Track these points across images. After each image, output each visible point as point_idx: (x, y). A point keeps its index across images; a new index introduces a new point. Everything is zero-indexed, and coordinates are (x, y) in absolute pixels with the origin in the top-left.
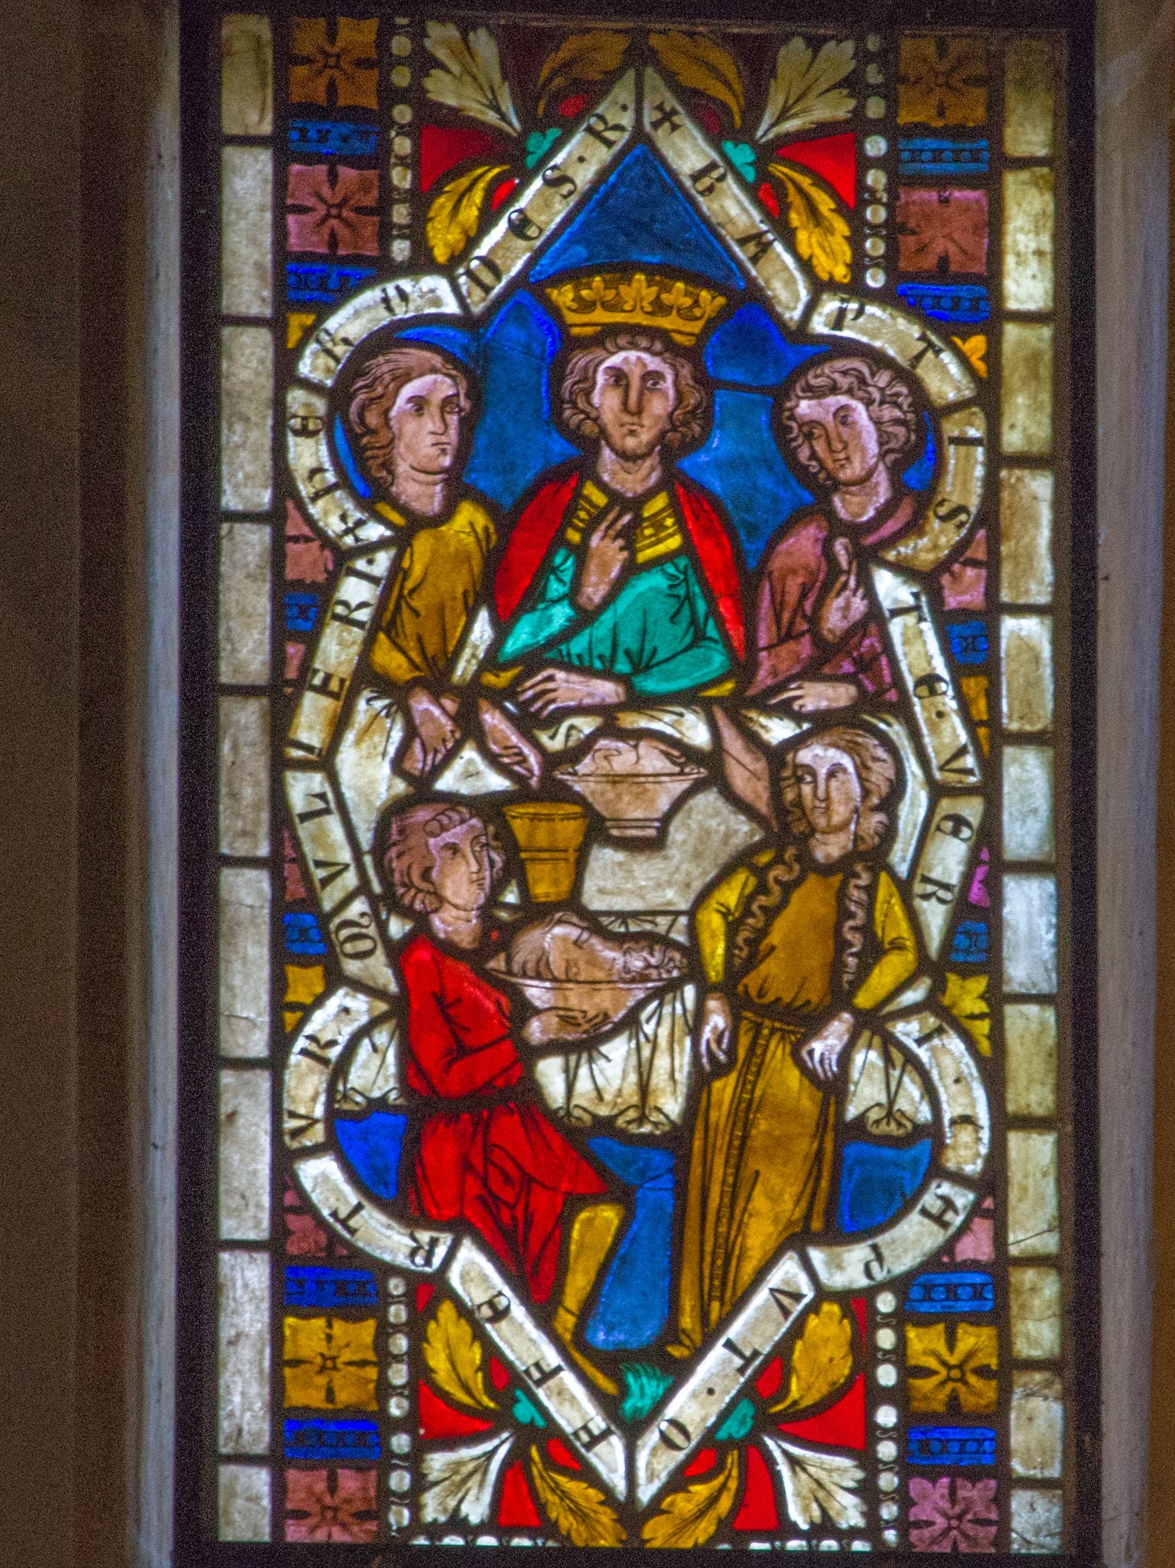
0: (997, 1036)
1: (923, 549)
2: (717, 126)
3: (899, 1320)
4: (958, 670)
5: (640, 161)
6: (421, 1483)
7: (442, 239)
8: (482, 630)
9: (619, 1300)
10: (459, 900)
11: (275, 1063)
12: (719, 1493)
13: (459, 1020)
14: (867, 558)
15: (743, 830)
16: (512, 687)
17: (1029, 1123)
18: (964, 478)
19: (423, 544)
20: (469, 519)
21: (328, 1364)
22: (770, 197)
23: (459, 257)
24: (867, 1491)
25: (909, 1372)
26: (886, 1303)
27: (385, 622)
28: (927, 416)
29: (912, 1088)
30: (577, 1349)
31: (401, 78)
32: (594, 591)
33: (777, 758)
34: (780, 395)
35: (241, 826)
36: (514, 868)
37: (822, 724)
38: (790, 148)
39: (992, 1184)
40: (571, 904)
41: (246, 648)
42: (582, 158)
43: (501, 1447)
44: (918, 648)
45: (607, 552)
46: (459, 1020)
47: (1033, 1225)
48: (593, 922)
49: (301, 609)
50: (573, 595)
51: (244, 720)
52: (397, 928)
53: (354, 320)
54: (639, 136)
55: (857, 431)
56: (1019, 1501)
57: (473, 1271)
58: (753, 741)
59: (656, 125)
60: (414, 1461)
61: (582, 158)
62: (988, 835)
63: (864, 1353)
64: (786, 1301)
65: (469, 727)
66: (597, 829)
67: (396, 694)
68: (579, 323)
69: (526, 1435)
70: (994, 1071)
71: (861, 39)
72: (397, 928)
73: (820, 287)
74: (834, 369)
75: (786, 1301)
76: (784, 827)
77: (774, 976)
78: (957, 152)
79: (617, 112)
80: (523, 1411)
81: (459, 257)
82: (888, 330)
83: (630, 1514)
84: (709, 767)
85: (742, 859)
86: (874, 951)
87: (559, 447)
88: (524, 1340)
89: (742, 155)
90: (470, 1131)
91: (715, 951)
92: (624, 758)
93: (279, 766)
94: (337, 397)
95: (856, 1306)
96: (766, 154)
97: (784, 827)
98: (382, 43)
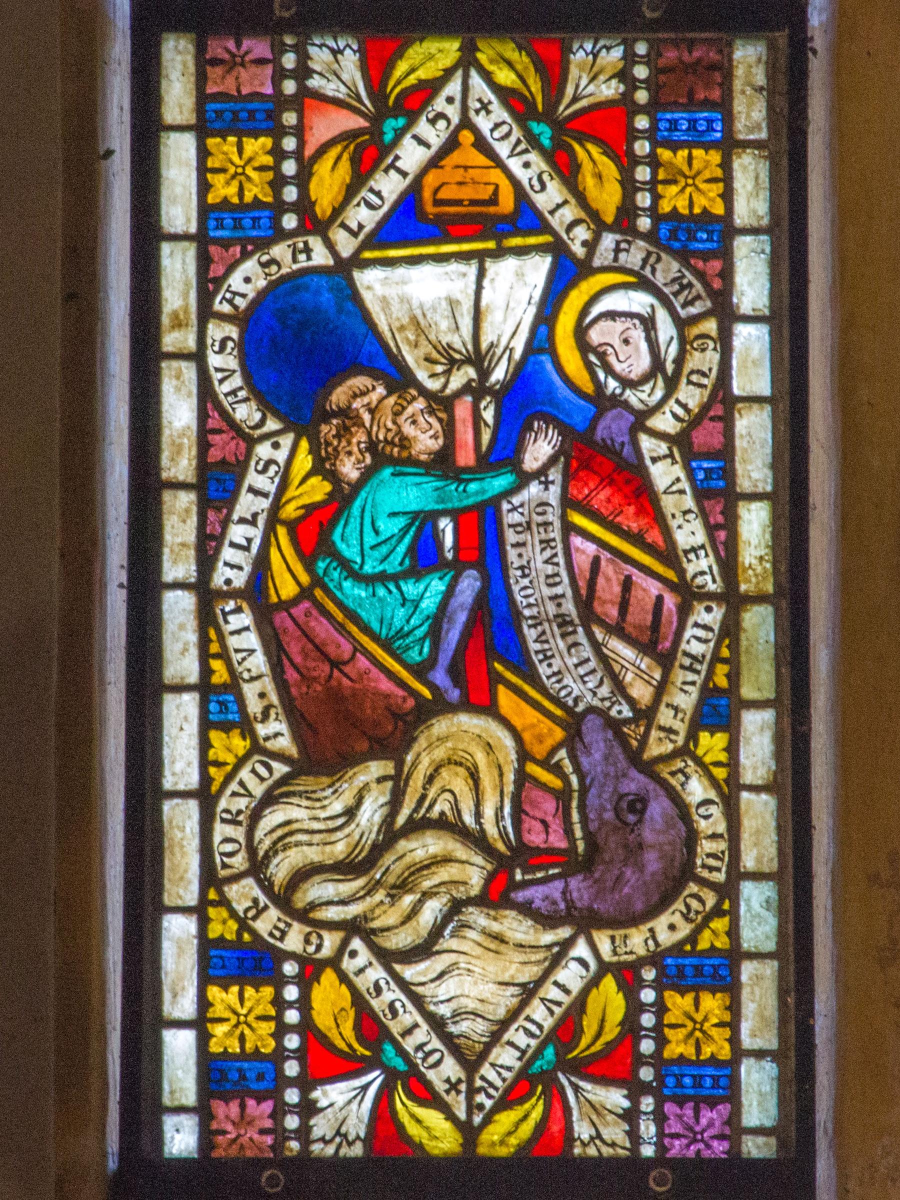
26: (649, 974)
59: (477, 112)
71: (629, 45)
95: (627, 975)
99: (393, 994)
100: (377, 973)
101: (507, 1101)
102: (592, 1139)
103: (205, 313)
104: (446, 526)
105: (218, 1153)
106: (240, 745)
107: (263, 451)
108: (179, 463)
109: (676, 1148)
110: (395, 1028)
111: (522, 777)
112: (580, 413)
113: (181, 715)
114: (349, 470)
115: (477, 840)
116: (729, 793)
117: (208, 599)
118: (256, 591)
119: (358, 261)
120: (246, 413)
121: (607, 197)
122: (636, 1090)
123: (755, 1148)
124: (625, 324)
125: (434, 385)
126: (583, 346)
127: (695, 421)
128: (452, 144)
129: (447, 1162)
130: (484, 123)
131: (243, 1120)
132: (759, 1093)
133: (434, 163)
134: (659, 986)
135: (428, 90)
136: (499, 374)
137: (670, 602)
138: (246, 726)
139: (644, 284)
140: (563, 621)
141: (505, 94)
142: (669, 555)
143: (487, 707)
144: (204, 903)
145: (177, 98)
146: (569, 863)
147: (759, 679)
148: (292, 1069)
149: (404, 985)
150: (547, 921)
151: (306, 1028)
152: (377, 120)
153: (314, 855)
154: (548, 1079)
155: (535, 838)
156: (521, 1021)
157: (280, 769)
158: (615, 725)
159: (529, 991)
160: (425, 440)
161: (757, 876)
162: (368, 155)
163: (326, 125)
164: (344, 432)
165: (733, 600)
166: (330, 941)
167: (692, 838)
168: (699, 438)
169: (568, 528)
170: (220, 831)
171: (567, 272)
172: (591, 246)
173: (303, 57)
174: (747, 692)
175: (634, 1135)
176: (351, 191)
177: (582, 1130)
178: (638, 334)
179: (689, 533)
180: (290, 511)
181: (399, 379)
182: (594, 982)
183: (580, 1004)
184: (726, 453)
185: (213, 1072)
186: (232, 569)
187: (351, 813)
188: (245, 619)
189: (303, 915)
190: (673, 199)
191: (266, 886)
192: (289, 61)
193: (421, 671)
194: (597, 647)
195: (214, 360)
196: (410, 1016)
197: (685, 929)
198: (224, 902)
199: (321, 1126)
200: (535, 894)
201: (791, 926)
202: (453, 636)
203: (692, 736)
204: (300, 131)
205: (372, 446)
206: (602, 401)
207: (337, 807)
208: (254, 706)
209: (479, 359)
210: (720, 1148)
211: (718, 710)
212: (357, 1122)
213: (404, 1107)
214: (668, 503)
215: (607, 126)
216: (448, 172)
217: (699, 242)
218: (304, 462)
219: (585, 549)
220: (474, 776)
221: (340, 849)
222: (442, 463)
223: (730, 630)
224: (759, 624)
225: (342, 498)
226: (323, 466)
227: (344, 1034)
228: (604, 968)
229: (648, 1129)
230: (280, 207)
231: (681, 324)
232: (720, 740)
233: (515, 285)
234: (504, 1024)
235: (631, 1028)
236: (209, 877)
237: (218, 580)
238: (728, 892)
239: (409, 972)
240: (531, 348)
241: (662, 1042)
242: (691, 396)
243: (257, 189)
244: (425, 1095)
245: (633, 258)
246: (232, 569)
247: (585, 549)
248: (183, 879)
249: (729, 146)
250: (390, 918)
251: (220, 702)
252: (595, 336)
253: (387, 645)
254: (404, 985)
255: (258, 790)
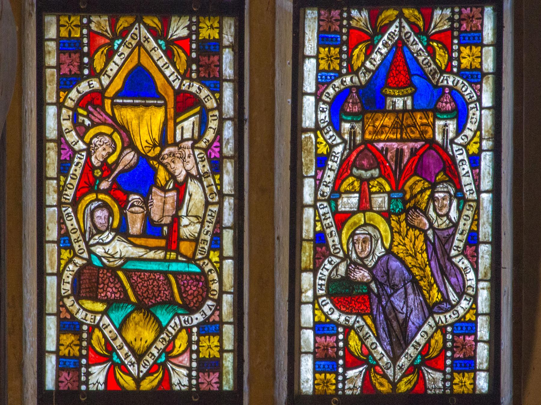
12: (413, 378)
24: (189, 376)
31: (345, 22)
59: (144, 41)
64: (360, 328)
75: (360, 328)
78: (474, 39)
98: (341, 14)
102: (178, 384)
105: (61, 389)
113: (51, 249)
129: (133, 391)
148: (84, 361)
154: (164, 364)
156: (163, 69)
165: (222, 120)
201: (237, 235)
213: (119, 374)
228: (182, 328)
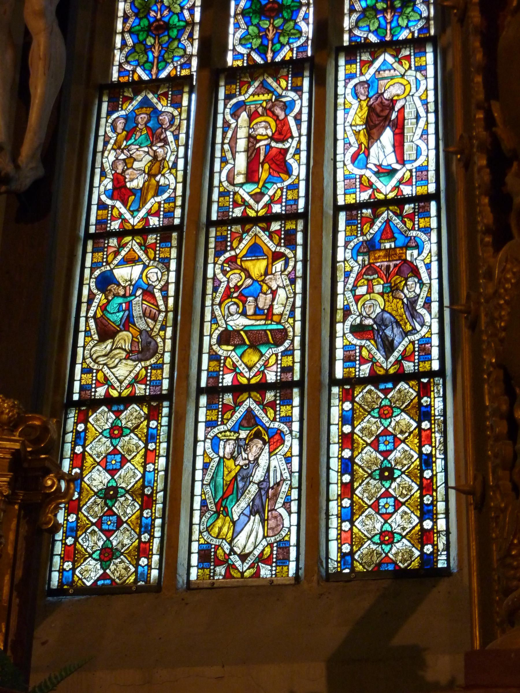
0: (176, 175)
1: (172, 129)
2: (154, 93)
3: (164, 204)
4: (175, 140)
5: (146, 98)
6: (111, 225)
7: (124, 108)
8: (125, 143)
9: (133, 205)
10: (120, 168)
11: (99, 187)
12: (143, 223)
13: (119, 182)
14: (166, 130)
15: (151, 158)
16: (127, 148)
17: (179, 183)
18: (177, 122)
19: (119, 136)
20: (125, 133)
21: (102, 215)
22: (159, 99)
23: (126, 109)
25: (164, 208)
26: (150, 368)
27: (115, 143)
28: (173, 117)
29: (167, 180)
30: (129, 210)
32: (137, 138)
33: (155, 152)
34: (158, 117)
35: (98, 165)
36: (126, 165)
37: (160, 147)
38: (161, 94)
39: (175, 189)
40: (132, 168)
41: (100, 147)
42: (139, 98)
43: (120, 221)
44: (170, 138)
45: (138, 134)
46: (119, 182)
47: (179, 192)
48: (134, 169)
49: (106, 143)
50: (135, 138)
51: (99, 155)
52: (113, 172)
53: (114, 116)
54: (146, 95)
55: (166, 119)
56: (175, 220)
57: (118, 204)
58: (152, 149)
60: (110, 223)
61: (139, 98)
62: (177, 156)
63: (160, 207)
65: (122, 152)
66: (135, 160)
67: (115, 150)
68: (138, 113)
69: (123, 219)
70: (176, 178)
72: (113, 172)
73: (163, 106)
74: (164, 114)
76: (155, 157)
77: (153, 172)
79: (143, 94)
80: (123, 217)
81: (126, 109)
82: (170, 109)
83: (133, 226)
84: (148, 153)
85: (151, 161)
86: (164, 168)
87: (135, 125)
88: (123, 210)
89: (156, 96)
90: (120, 191)
91: (147, 171)
92: (138, 153)
93: (102, 158)
94: (112, 124)
95: (146, 368)
96: (158, 95)
97: (155, 157)
99: (110, 374)
100: (108, 371)
101: (126, 388)
103: (91, 278)
104: (124, 305)
106: (90, 339)
107: (97, 296)
108: (85, 299)
109: (152, 393)
110: (110, 379)
111: (132, 340)
112: (145, 287)
113: (81, 335)
114: (110, 298)
115: (125, 350)
116: (164, 340)
117: (87, 318)
118: (94, 317)
119: (114, 268)
120: (95, 291)
121: (152, 256)
122: (146, 385)
123: (164, 392)
124: (154, 274)
125: (123, 285)
126: (147, 277)
127: (163, 287)
128: (129, 251)
130: (134, 248)
131: (86, 394)
132: (166, 384)
133: (127, 254)
134: (151, 369)
135: (127, 244)
136: (133, 283)
137: (157, 313)
138: (91, 336)
139: (156, 267)
140: (140, 317)
141: (138, 243)
142: (157, 306)
143: (128, 330)
144: (82, 362)
145: (90, 248)
146: (139, 352)
147: (170, 322)
149: (112, 372)
150: (134, 361)
151: (96, 380)
152: (118, 249)
153: (100, 354)
155: (134, 349)
157: (96, 342)
158: (147, 332)
159: (131, 372)
160: (122, 292)
161: (167, 352)
162: (117, 253)
163: (111, 250)
164: (110, 293)
166: (101, 367)
167: (158, 347)
168: (163, 289)
169: (142, 303)
170: (86, 352)
171: (145, 267)
172: (149, 263)
173: (108, 241)
174: (168, 325)
175: (145, 392)
176: (114, 259)
177: (137, 392)
178: (155, 275)
179: (161, 302)
180: (101, 305)
181: (119, 285)
182: (141, 369)
183: (138, 373)
184: (167, 290)
185: (82, 387)
186: (91, 314)
187: (106, 348)
188: (93, 320)
189: (97, 363)
190: (162, 255)
191: (92, 359)
192: (106, 242)
193: (118, 326)
194: (145, 320)
195: (91, 284)
196: (112, 376)
197: (155, 361)
198: (85, 362)
199: (97, 394)
200: (133, 357)
202: (123, 320)
203: (159, 332)
204: (107, 251)
205: (114, 294)
206: (149, 285)
207: (104, 347)
208: (92, 333)
209: (131, 280)
210: (159, 393)
211: (163, 328)
212: (103, 393)
213: (110, 390)
214: (158, 299)
215: (153, 246)
216: (128, 255)
217: (165, 262)
218: (103, 297)
219: (144, 306)
220: (125, 341)
221: (104, 353)
222: (124, 296)
223: (166, 316)
224: (171, 315)
225: (109, 302)
226: (106, 298)
227: (102, 380)
228: (143, 367)
229: (148, 391)
230: (103, 262)
231: (162, 273)
232: (163, 332)
233: (138, 268)
234: (126, 377)
235: (146, 376)
236: (84, 359)
237: (89, 315)
238: (163, 355)
239: (113, 370)
240: (139, 278)
241: (151, 377)
242: (162, 283)
243: (100, 260)
244: (114, 388)
245: (155, 264)
246: (91, 314)
247: (144, 306)
248: (79, 359)
249: (171, 247)
250: (111, 362)
251: (87, 332)
252: (148, 276)
253: (113, 323)
254: (112, 372)
255: (92, 345)
